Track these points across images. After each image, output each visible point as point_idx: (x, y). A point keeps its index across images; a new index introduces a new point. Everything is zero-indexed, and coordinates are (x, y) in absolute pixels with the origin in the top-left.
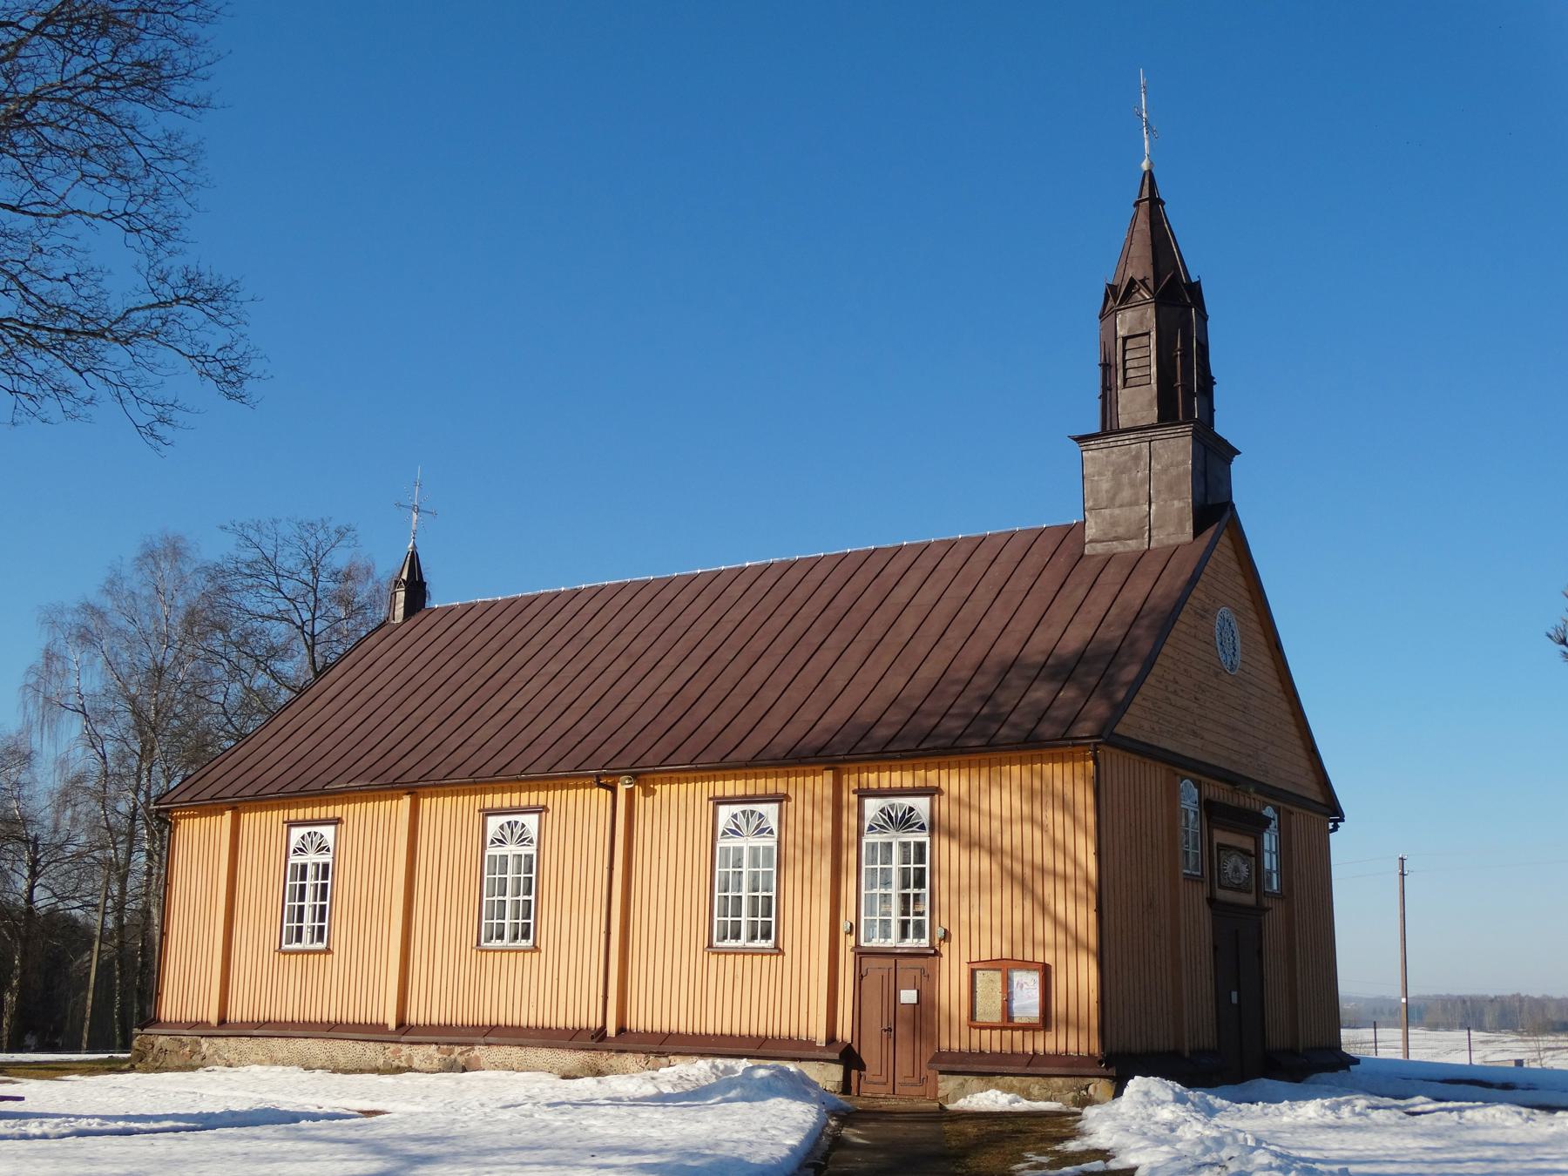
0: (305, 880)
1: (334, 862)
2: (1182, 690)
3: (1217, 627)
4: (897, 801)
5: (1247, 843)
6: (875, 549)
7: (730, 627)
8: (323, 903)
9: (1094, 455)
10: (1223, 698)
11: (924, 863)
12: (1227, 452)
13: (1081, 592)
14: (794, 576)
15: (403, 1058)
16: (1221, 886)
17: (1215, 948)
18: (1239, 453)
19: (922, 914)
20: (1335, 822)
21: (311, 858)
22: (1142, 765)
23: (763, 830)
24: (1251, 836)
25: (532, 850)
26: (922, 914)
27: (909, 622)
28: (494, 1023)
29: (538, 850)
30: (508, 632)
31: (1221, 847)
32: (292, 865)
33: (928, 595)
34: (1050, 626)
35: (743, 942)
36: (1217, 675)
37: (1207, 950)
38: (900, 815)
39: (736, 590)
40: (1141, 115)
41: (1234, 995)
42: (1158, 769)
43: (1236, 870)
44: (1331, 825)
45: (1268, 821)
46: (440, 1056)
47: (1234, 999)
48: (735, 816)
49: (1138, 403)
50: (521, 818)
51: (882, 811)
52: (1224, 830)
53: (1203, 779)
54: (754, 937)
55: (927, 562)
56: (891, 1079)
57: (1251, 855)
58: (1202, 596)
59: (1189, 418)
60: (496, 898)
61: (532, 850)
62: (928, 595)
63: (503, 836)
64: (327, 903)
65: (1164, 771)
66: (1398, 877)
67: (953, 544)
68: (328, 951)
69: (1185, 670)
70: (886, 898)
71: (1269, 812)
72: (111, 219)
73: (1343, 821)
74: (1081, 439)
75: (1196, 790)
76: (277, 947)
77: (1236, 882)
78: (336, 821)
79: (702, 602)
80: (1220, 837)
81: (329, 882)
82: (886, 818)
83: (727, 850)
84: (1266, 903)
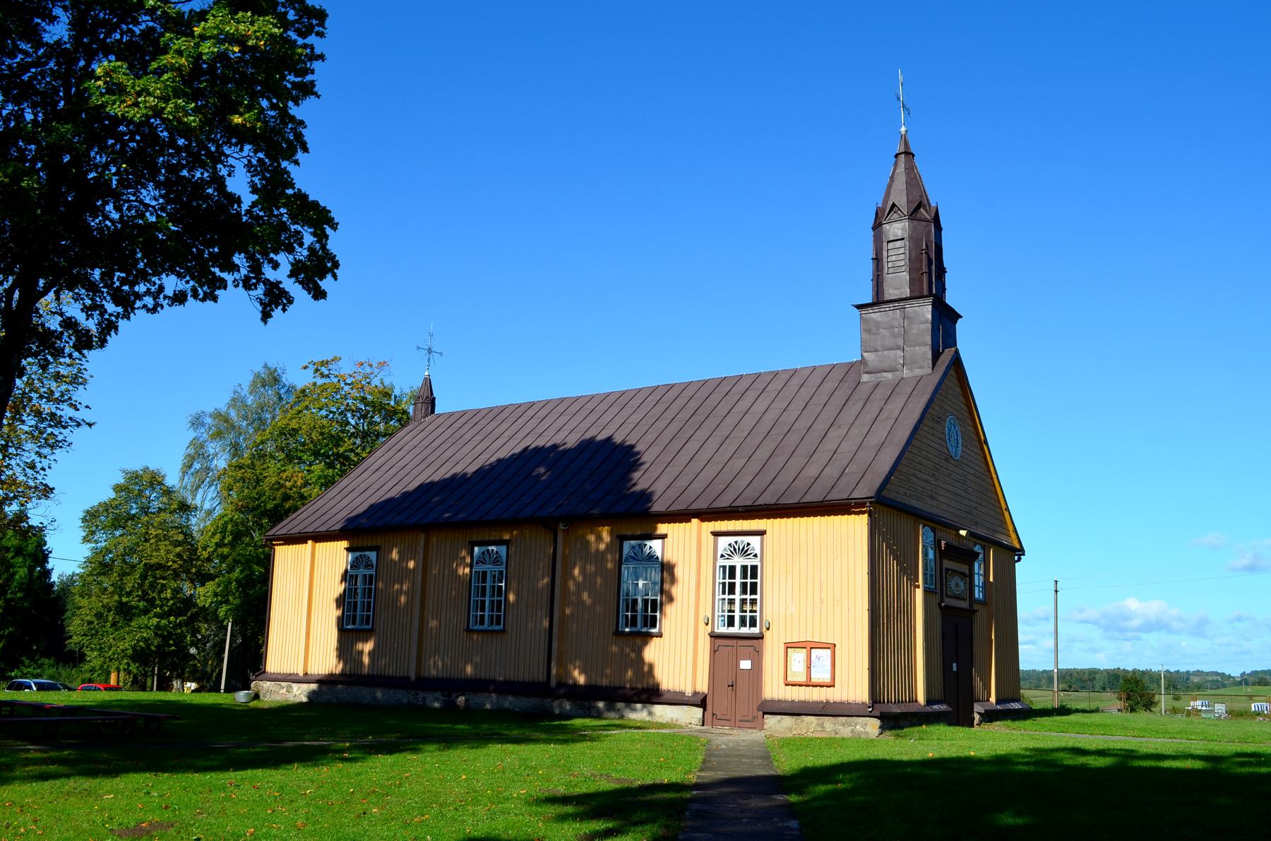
0: (735, 578)
1: (376, 574)
2: (925, 469)
3: (947, 429)
4: (739, 539)
5: (965, 569)
6: (725, 378)
7: (632, 426)
8: (753, 597)
9: (875, 315)
10: (950, 474)
11: (757, 579)
12: (953, 316)
13: (860, 405)
14: (673, 393)
15: (420, 699)
16: (947, 596)
17: (943, 635)
18: (961, 317)
19: (755, 611)
20: (1019, 556)
21: (738, 561)
22: (899, 517)
23: (369, 566)
24: (967, 564)
25: (503, 568)
26: (755, 611)
27: (749, 422)
28: (292, 672)
29: (376, 571)
30: (489, 428)
31: (947, 570)
32: (475, 572)
33: (760, 407)
34: (839, 426)
35: (486, 626)
36: (946, 460)
37: (938, 637)
38: (741, 548)
39: (636, 402)
40: (899, 99)
41: (955, 666)
42: (909, 520)
43: (957, 585)
44: (1016, 558)
45: (978, 554)
46: (443, 698)
47: (955, 668)
48: (633, 547)
49: (898, 282)
50: (367, 553)
51: (730, 545)
52: (950, 560)
53: (937, 526)
54: (492, 624)
55: (759, 385)
56: (733, 717)
57: (967, 576)
58: (938, 409)
59: (930, 294)
60: (479, 599)
61: (756, 562)
62: (760, 407)
63: (484, 559)
64: (757, 597)
65: (912, 521)
66: (1053, 592)
67: (776, 374)
68: (504, 631)
69: (926, 456)
70: (731, 602)
71: (977, 549)
72: (238, 159)
73: (1024, 555)
74: (859, 307)
75: (933, 534)
76: (465, 628)
77: (957, 593)
78: (761, 533)
79: (614, 410)
80: (947, 564)
81: (758, 581)
82: (732, 549)
83: (724, 567)
84: (976, 607)
